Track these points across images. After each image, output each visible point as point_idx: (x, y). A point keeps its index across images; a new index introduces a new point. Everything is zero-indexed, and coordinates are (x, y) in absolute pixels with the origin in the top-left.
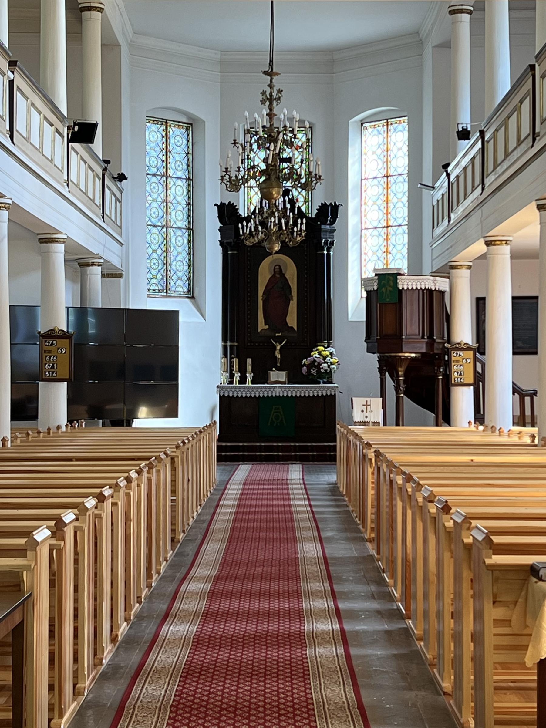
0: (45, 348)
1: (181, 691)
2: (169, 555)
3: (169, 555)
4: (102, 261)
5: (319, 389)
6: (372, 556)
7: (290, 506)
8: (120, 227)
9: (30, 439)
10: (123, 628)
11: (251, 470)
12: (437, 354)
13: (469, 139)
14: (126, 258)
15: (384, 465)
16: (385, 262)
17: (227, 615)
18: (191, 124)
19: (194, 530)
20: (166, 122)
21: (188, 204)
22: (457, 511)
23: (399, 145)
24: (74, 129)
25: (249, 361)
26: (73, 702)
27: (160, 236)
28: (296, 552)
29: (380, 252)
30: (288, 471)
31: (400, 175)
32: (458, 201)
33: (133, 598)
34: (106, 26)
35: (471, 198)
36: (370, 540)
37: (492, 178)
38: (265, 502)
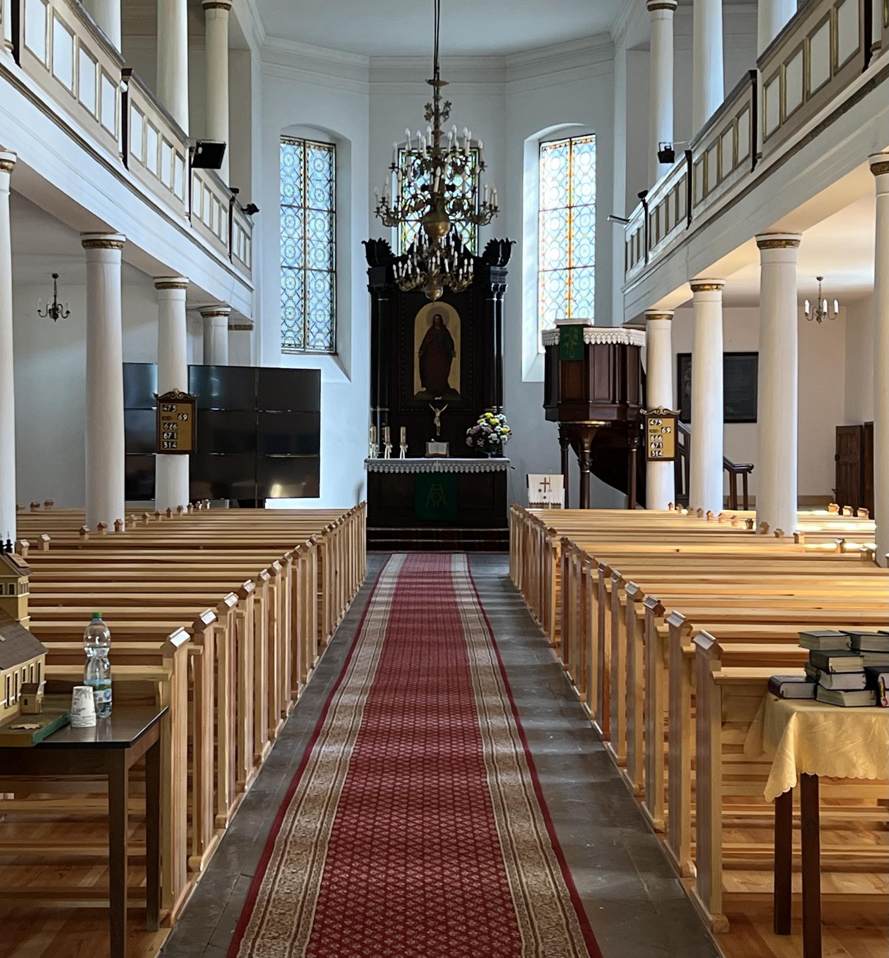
1: (340, 824)
2: (315, 662)
3: (315, 662)
4: (229, 310)
5: (488, 463)
6: (557, 665)
7: (456, 603)
8: (250, 269)
9: (147, 522)
10: (267, 748)
11: (406, 561)
12: (630, 422)
13: (672, 161)
15: (574, 556)
16: (567, 311)
17: (389, 734)
18: (335, 145)
19: (342, 632)
20: (304, 143)
21: (331, 242)
22: (673, 613)
23: (585, 169)
24: (197, 151)
25: (403, 430)
26: (213, 836)
27: (297, 280)
28: (466, 661)
29: (560, 298)
30: (450, 562)
31: (586, 205)
33: (277, 714)
36: (555, 646)
37: (701, 208)
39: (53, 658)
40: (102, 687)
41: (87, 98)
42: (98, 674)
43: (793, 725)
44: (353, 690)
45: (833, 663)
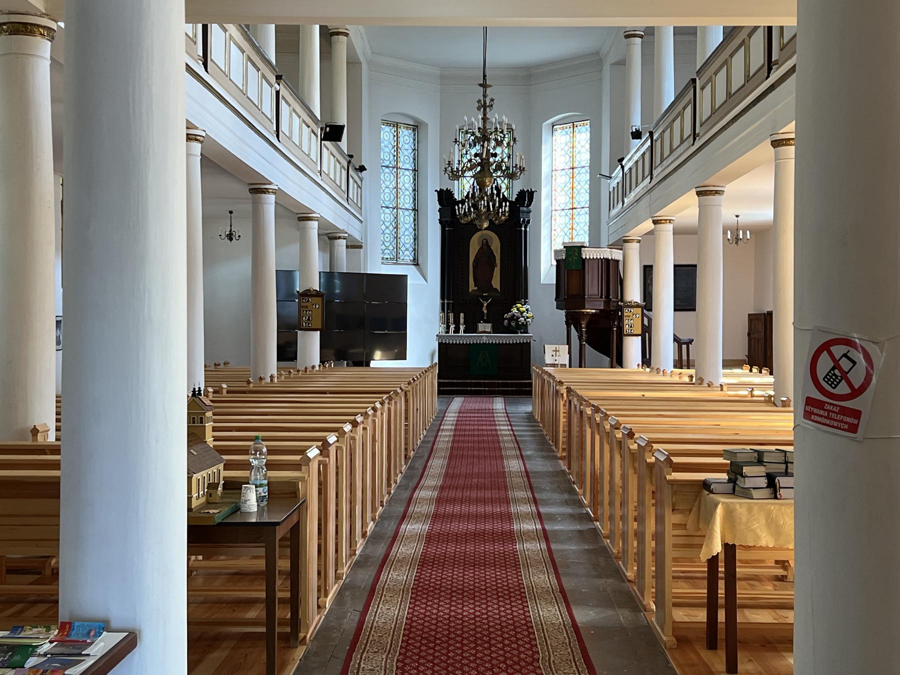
0: (303, 304)
6: (564, 471)
7: (496, 430)
14: (365, 233)
15: (575, 399)
17: (452, 517)
21: (414, 190)
23: (583, 143)
25: (462, 315)
28: (503, 467)
32: (631, 189)
33: (377, 503)
34: (350, 48)
35: (641, 186)
36: (562, 458)
37: (659, 169)
38: (476, 427)
39: (228, 466)
40: (261, 485)
41: (253, 94)
42: (258, 477)
43: (719, 511)
44: (428, 488)
45: (745, 470)
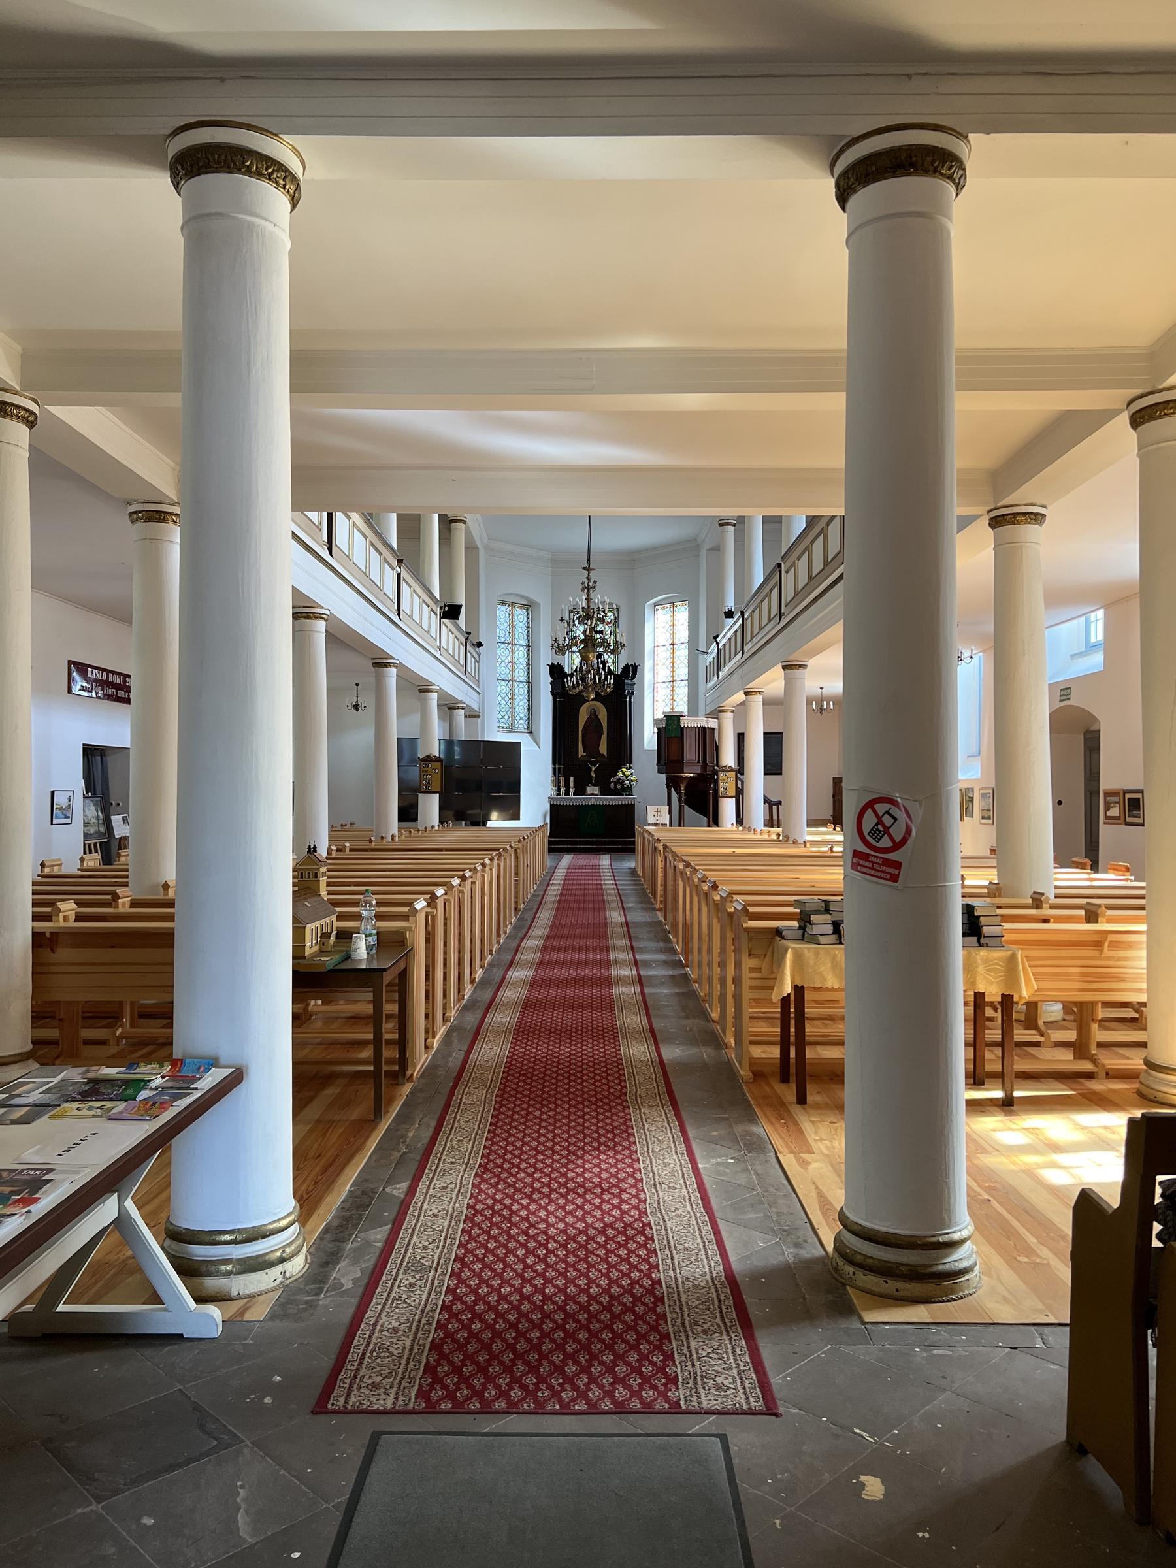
5: (622, 800)
10: (479, 973)
33: (486, 951)
34: (468, 534)
36: (659, 910)
37: (749, 646)
39: (341, 917)
40: (371, 935)
41: (375, 576)
42: (368, 927)
43: (789, 955)
44: (535, 938)
45: (813, 918)
